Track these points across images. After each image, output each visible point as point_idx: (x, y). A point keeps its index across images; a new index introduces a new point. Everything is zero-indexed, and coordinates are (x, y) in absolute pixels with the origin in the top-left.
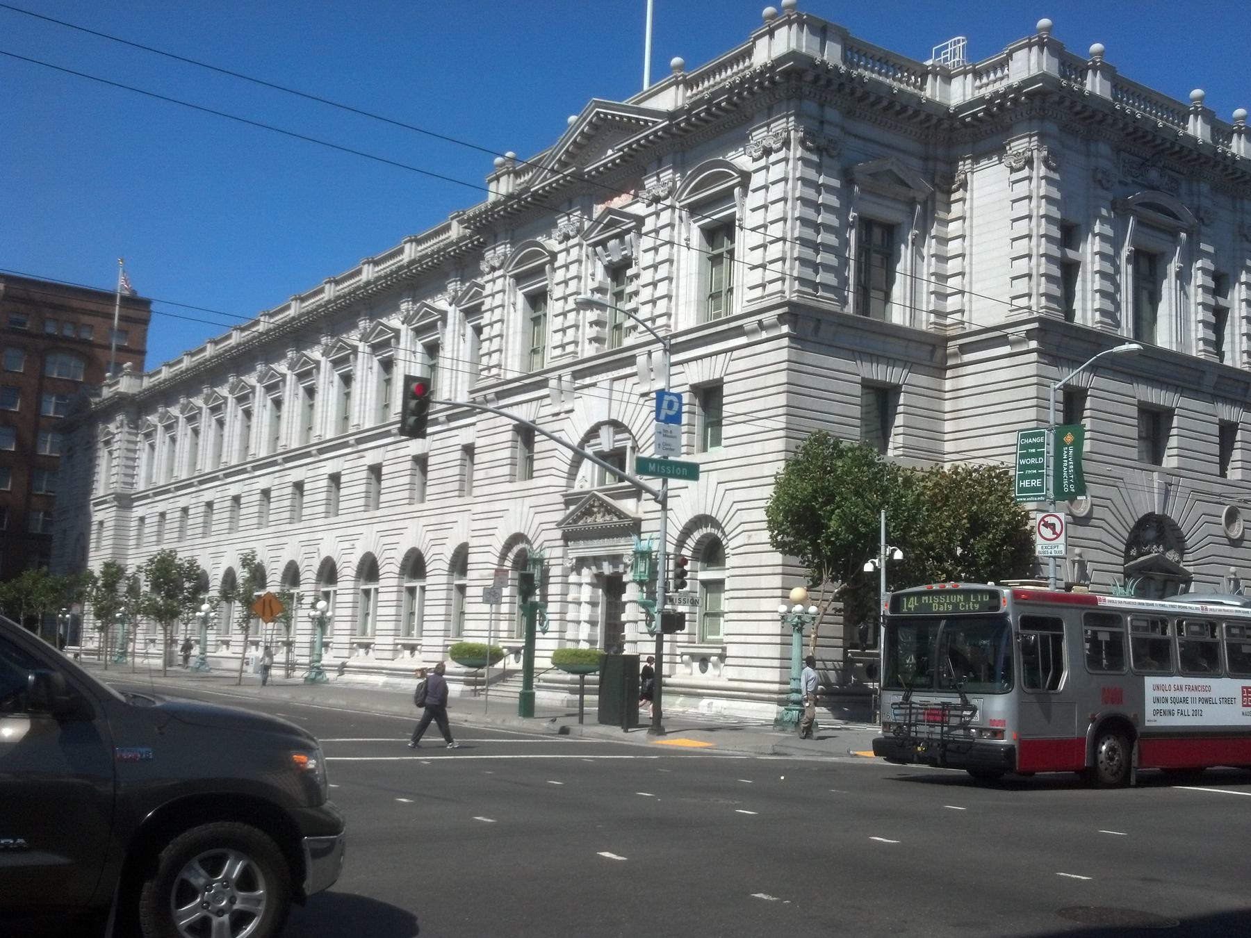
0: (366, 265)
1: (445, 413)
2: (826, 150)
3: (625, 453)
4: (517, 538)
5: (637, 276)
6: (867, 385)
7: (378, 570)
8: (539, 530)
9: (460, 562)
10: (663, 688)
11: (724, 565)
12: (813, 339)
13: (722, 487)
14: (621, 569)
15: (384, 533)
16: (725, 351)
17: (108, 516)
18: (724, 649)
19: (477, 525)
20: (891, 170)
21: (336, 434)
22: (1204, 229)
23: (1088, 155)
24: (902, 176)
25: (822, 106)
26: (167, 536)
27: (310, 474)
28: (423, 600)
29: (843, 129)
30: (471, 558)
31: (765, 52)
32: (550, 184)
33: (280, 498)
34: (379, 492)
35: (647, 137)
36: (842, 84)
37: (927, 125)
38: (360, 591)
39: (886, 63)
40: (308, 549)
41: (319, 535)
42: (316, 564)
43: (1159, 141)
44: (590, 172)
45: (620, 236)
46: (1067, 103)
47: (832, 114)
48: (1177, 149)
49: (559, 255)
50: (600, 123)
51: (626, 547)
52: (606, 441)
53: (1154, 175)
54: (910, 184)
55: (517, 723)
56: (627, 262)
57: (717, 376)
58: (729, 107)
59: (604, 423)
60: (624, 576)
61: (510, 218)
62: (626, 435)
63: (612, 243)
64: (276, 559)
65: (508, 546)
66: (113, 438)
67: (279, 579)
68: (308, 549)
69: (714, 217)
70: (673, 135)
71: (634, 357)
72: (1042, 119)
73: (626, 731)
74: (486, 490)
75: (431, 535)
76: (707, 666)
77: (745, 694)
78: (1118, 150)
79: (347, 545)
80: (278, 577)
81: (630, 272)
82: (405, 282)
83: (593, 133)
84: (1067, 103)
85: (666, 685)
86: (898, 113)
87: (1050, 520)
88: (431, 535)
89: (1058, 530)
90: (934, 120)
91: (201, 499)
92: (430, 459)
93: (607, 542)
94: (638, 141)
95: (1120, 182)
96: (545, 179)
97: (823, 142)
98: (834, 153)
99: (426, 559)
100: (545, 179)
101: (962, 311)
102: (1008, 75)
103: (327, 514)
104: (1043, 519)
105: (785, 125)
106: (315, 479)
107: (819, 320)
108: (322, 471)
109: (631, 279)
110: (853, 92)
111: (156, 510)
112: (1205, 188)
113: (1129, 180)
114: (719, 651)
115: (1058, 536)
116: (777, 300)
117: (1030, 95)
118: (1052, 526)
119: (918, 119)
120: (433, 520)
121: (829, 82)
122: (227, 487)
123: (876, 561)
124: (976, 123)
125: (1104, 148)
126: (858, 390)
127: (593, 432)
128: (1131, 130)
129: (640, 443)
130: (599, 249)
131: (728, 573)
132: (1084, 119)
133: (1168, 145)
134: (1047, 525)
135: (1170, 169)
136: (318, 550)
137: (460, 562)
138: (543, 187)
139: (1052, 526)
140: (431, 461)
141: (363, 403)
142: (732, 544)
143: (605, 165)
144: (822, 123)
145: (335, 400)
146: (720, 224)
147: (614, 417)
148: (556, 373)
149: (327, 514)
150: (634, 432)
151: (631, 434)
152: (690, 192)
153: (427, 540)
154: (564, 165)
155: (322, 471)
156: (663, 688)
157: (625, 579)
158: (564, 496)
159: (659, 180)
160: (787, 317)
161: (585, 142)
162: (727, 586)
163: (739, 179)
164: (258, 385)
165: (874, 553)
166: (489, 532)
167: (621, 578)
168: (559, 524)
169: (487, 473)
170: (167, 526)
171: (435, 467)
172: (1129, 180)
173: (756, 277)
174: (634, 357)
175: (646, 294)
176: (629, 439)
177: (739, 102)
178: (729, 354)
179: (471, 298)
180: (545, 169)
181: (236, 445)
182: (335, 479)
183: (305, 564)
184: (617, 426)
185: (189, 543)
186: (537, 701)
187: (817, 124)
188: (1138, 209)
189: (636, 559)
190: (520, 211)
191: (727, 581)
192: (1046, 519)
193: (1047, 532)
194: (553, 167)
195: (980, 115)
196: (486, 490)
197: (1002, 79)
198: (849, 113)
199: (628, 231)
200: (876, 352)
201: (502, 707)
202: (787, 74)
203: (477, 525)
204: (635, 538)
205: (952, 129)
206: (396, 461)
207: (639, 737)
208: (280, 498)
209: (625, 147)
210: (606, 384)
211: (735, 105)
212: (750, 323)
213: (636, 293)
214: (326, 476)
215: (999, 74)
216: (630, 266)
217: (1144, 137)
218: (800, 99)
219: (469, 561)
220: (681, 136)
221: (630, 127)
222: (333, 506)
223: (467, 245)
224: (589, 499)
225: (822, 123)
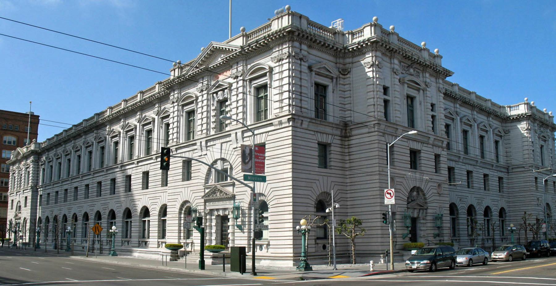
0: (123, 102)
1: (155, 156)
2: (303, 59)
3: (228, 170)
4: (186, 202)
5: (230, 104)
6: (319, 144)
7: (131, 214)
8: (194, 199)
9: (164, 211)
10: (246, 257)
11: (268, 211)
12: (300, 127)
13: (192, 192)
14: (227, 213)
15: (79, 207)
16: (266, 132)
17: (29, 195)
18: (269, 242)
19: (170, 197)
20: (324, 67)
21: (87, 171)
22: (428, 89)
23: (391, 63)
24: (329, 69)
25: (301, 44)
26: (50, 202)
27: (104, 179)
28: (149, 225)
29: (308, 52)
30: (168, 210)
31: (276, 26)
32: (196, 72)
33: (93, 188)
34: (130, 185)
35: (233, 55)
36: (307, 37)
37: (336, 51)
38: (124, 222)
39: (321, 29)
40: (104, 206)
41: (107, 201)
42: (107, 212)
43: (413, 59)
44: (211, 67)
45: (223, 90)
46: (384, 46)
47: (304, 47)
48: (419, 62)
49: (199, 97)
50: (214, 50)
51: (229, 205)
52: (219, 166)
53: (412, 70)
54: (331, 72)
55: (199, 272)
56: (226, 100)
57: (263, 142)
58: (264, 44)
59: (219, 159)
60: (229, 216)
61: (180, 84)
62: (228, 163)
63: (220, 93)
64: (92, 210)
65: (182, 205)
66: (30, 166)
67: (157, 213)
68: (104, 206)
69: (259, 84)
70: (243, 54)
71: (230, 134)
72: (376, 51)
73: (242, 274)
74: (173, 184)
75: (151, 201)
76: (262, 249)
77: (318, 257)
78: (400, 62)
79: (119, 205)
80: (93, 217)
81: (227, 103)
82: (139, 108)
83: (211, 53)
84: (384, 46)
85: (247, 256)
86: (327, 47)
87: (389, 192)
88: (151, 201)
89: (392, 195)
90: (339, 50)
91: (63, 188)
92: (150, 173)
93: (221, 203)
94: (230, 56)
95: (402, 73)
96: (193, 70)
97: (301, 56)
98: (305, 60)
99: (150, 210)
100: (193, 70)
101: (351, 117)
102: (363, 35)
103: (85, 198)
104: (387, 191)
105: (278, 54)
106: (93, 184)
107: (302, 120)
108: (108, 178)
109: (227, 106)
110: (311, 40)
111: (54, 190)
112: (427, 75)
113: (404, 72)
114: (267, 243)
115: (392, 197)
116: (287, 113)
117: (371, 42)
118: (390, 194)
119: (333, 49)
120: (59, 208)
121: (303, 35)
122: (73, 184)
123: (331, 208)
124: (353, 51)
125: (396, 61)
126: (317, 146)
127: (215, 162)
128: (404, 55)
129: (233, 167)
130: (215, 95)
131: (269, 214)
132: (390, 51)
133: (416, 60)
134: (388, 193)
135: (417, 69)
136: (108, 206)
137: (164, 211)
138: (193, 73)
139: (390, 194)
140: (150, 174)
141: (73, 166)
142: (271, 204)
143: (217, 65)
144: (301, 50)
145: (99, 156)
146: (260, 86)
147: (222, 157)
148: (199, 141)
149: (163, 185)
150: (230, 162)
151: (230, 163)
152: (249, 75)
153: (150, 203)
154: (201, 65)
155: (108, 178)
156: (246, 257)
157: (229, 217)
158: (204, 186)
159: (237, 70)
160: (291, 119)
161: (209, 57)
162: (269, 219)
163: (268, 70)
164: (95, 141)
165: (330, 205)
166: (69, 212)
167: (228, 216)
168: (203, 197)
169: (173, 178)
170: (59, 197)
171: (133, 180)
172: (404, 72)
173: (277, 105)
174: (230, 134)
175: (234, 111)
176: (229, 165)
177: (267, 43)
178: (267, 133)
179: (164, 113)
180: (193, 67)
181: (75, 168)
182: (87, 186)
183: (103, 212)
184: (223, 160)
185: (80, 201)
186: (206, 263)
187: (299, 50)
188: (408, 82)
189: (234, 209)
190: (183, 81)
191: (269, 217)
192: (388, 191)
193: (388, 196)
194: (196, 66)
195: (355, 48)
196: (173, 184)
197: (361, 36)
198: (310, 47)
199: (226, 88)
200: (322, 132)
201: (192, 266)
202: (289, 32)
203: (170, 197)
204: (232, 201)
205: (345, 53)
206: (137, 174)
207: (247, 276)
208: (93, 188)
209: (224, 58)
210: (219, 146)
211: (266, 44)
212: (276, 122)
213: (230, 111)
214: (110, 180)
215: (360, 35)
216: (227, 101)
217: (408, 58)
218: (293, 41)
219: (167, 211)
220: (245, 55)
221: (229, 51)
222: (87, 196)
223: (158, 96)
224: (214, 187)
225: (301, 50)
